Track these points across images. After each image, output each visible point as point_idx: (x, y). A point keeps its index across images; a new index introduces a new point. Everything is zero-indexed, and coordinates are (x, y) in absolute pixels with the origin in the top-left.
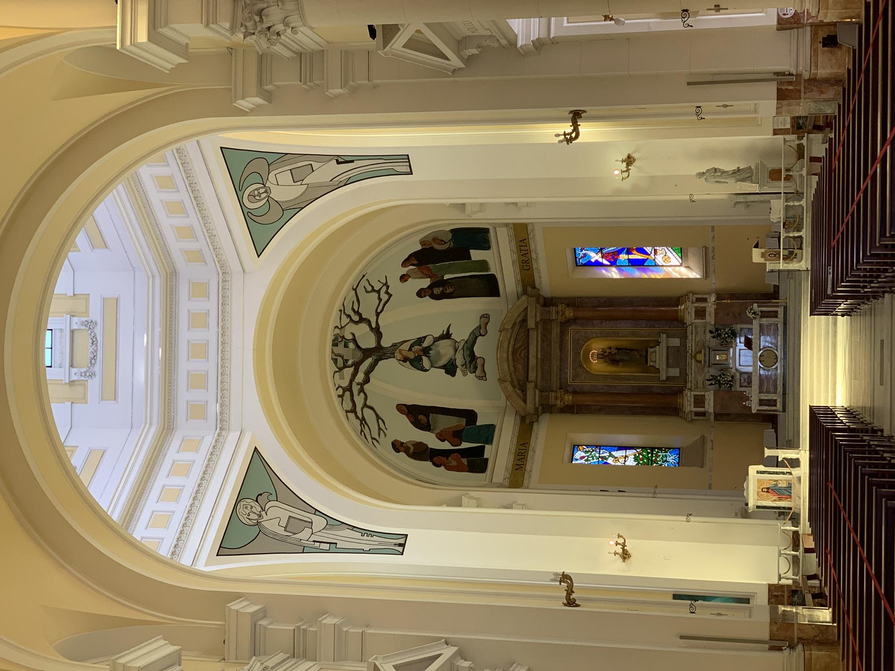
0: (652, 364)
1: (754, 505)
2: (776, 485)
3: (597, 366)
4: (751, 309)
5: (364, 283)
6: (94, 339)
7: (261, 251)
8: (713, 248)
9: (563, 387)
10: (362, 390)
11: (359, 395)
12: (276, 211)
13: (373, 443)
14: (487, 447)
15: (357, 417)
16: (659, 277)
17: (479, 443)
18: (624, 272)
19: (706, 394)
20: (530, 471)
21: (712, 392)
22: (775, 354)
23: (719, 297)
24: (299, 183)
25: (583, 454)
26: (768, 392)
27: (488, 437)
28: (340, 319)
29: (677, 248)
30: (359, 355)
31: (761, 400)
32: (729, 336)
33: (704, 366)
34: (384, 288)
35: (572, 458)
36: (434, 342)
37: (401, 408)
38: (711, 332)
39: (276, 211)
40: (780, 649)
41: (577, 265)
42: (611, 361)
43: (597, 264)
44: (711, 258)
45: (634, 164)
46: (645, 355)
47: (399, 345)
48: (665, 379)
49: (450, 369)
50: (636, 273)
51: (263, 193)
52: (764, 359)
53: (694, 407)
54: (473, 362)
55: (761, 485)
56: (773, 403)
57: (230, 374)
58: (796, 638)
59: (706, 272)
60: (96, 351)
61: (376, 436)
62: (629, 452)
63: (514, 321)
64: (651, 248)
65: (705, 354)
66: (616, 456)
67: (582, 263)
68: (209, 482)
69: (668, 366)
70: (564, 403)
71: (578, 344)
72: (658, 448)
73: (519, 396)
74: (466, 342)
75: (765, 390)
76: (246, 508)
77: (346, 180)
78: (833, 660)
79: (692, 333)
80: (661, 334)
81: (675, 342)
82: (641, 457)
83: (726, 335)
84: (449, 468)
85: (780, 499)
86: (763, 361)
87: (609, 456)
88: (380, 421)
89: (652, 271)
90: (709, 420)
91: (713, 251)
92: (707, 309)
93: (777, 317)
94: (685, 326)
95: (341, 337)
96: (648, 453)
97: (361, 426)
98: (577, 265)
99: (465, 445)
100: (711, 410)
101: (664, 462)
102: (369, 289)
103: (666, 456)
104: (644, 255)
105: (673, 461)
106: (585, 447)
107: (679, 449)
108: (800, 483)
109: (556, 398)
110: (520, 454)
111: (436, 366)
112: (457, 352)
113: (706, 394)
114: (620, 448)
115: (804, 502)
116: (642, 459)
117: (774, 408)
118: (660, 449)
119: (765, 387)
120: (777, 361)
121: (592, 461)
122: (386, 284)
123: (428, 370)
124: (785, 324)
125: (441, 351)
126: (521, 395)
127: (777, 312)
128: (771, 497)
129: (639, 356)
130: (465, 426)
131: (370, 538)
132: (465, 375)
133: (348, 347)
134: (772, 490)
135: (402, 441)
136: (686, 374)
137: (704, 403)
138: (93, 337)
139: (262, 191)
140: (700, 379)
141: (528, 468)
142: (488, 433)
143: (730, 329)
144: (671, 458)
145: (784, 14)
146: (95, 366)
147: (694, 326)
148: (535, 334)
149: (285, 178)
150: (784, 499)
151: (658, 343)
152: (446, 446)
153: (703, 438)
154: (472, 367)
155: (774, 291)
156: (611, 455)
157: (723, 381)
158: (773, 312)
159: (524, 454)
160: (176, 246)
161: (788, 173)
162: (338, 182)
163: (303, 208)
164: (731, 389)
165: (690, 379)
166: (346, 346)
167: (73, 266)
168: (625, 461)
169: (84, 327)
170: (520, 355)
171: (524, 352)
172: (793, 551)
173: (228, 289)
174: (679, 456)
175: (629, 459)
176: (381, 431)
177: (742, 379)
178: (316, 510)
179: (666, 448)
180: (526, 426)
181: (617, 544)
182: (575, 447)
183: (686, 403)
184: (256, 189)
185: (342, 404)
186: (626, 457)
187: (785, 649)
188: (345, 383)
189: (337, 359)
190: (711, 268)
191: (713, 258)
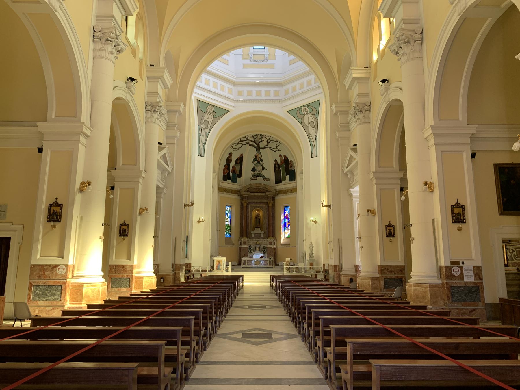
0: (255, 229)
5: (279, 144)
8: (290, 247)
10: (247, 143)
12: (300, 117)
14: (230, 181)
15: (239, 142)
23: (275, 249)
25: (229, 209)
31: (245, 261)
34: (277, 150)
38: (265, 246)
39: (300, 117)
40: (173, 267)
43: (285, 213)
49: (254, 170)
50: (282, 224)
54: (256, 176)
56: (244, 264)
60: (258, 62)
69: (255, 234)
71: (261, 207)
81: (262, 236)
85: (216, 267)
89: (283, 229)
90: (239, 246)
91: (289, 247)
93: (244, 265)
96: (229, 228)
99: (231, 174)
100: (242, 246)
102: (277, 145)
113: (247, 245)
114: (230, 220)
117: (243, 265)
118: (230, 232)
122: (279, 150)
124: (268, 268)
132: (252, 174)
136: (252, 239)
137: (244, 244)
139: (307, 112)
140: (251, 243)
142: (235, 181)
144: (228, 235)
145: (458, 270)
149: (311, 120)
151: (262, 231)
152: (231, 169)
154: (254, 176)
156: (228, 217)
160: (290, 86)
166: (260, 138)
169: (265, 58)
180: (237, 192)
181: (202, 219)
182: (231, 207)
183: (244, 239)
186: (228, 222)
188: (249, 138)
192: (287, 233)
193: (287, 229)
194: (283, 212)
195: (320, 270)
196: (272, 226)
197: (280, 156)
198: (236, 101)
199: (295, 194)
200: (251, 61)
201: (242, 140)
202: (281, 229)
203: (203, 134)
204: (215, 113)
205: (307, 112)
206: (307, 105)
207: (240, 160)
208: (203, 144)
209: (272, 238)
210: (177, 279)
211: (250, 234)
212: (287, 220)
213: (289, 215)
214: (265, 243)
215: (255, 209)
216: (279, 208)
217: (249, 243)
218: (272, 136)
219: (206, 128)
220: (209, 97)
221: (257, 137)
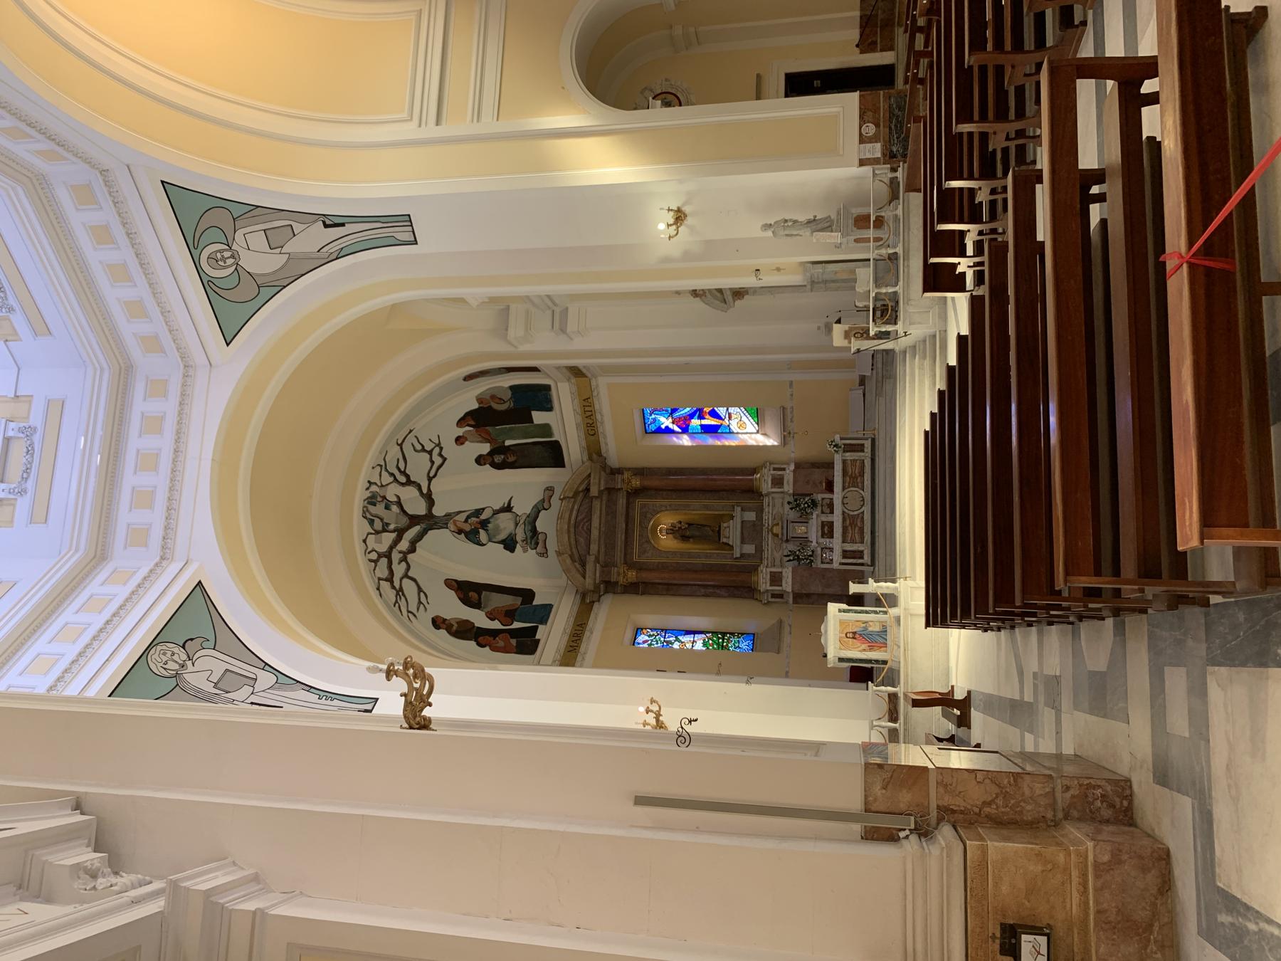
0: (725, 540)
1: (834, 656)
2: (865, 629)
3: (666, 542)
5: (411, 439)
6: (30, 449)
7: (232, 337)
8: (792, 408)
9: (631, 565)
10: (404, 559)
11: (399, 563)
12: (248, 289)
13: (408, 617)
14: (541, 627)
15: (393, 587)
17: (530, 623)
18: (696, 440)
20: (585, 653)
21: (790, 569)
24: (278, 250)
25: (647, 638)
26: (853, 541)
27: (544, 616)
28: (380, 476)
30: (404, 521)
31: (844, 551)
32: (809, 506)
34: (437, 450)
35: (634, 642)
36: (494, 514)
37: (449, 583)
38: (789, 503)
39: (248, 289)
40: (891, 837)
41: (646, 433)
43: (668, 431)
44: (789, 420)
45: (685, 222)
47: (453, 515)
48: (738, 555)
49: (509, 545)
50: (710, 441)
51: (228, 258)
53: (771, 585)
54: (534, 538)
55: (845, 628)
56: (860, 554)
57: (181, 490)
58: (933, 806)
60: (31, 463)
61: (413, 608)
66: (683, 640)
68: (123, 619)
69: (743, 542)
70: (627, 580)
71: (645, 517)
72: (730, 633)
73: (579, 571)
74: (528, 516)
76: (164, 654)
77: (337, 252)
78: (1049, 866)
79: (769, 505)
80: (735, 507)
81: (751, 516)
82: (711, 642)
83: (806, 505)
84: (494, 649)
85: (871, 648)
86: (847, 504)
87: (675, 641)
88: (422, 594)
89: (726, 439)
90: (787, 602)
91: (792, 412)
92: (785, 478)
93: (863, 451)
94: (762, 498)
95: (381, 497)
96: (719, 638)
97: (396, 597)
98: (646, 433)
99: (516, 625)
100: (789, 590)
102: (419, 447)
103: (739, 642)
107: (754, 634)
108: (899, 625)
109: (619, 574)
111: (494, 540)
113: (784, 571)
114: (688, 632)
115: (905, 650)
117: (860, 561)
118: (732, 634)
119: (850, 535)
120: (864, 504)
121: (656, 646)
122: (439, 445)
123: (485, 545)
124: (873, 460)
125: (501, 525)
126: (580, 569)
127: (863, 445)
128: (859, 645)
130: (521, 605)
131: (329, 702)
132: (525, 551)
133: (390, 510)
134: (860, 635)
135: (445, 618)
136: (762, 551)
137: (781, 581)
138: (30, 446)
139: (227, 254)
140: (778, 555)
141: (582, 649)
142: (544, 614)
144: (745, 645)
145: (867, 126)
146: (28, 482)
147: (771, 498)
148: (599, 504)
149: (258, 241)
150: (876, 648)
151: (732, 517)
152: (496, 625)
153: (781, 622)
154: (533, 543)
158: (858, 445)
160: (129, 329)
161: (878, 214)
162: (328, 254)
163: (285, 287)
164: (811, 565)
166: (387, 508)
167: (18, 362)
168: (693, 646)
169: (22, 435)
170: (583, 527)
171: (586, 524)
172: (889, 721)
173: (190, 385)
176: (422, 605)
178: (266, 664)
179: (739, 634)
180: (587, 603)
181: (648, 711)
182: (639, 630)
183: (761, 581)
184: (220, 251)
185: (374, 570)
186: (694, 641)
187: (907, 837)
188: (383, 548)
189: (374, 520)
191: (792, 421)
192: (741, 426)
193: (726, 420)
194: (665, 437)
195: (888, 182)
196: (715, 477)
197: (462, 440)
198: (165, 556)
199: (597, 386)
200: (22, 492)
201: (385, 574)
202: (727, 443)
203: (279, 698)
204: (192, 639)
205: (227, 254)
206: (193, 246)
207: (468, 592)
208: (323, 701)
210: (1006, 796)
211: (744, 562)
212: (695, 422)
214: (777, 507)
215: (652, 542)
216: (649, 452)
217: (777, 562)
218: (372, 456)
219: (252, 682)
220: (106, 658)
221: (382, 520)
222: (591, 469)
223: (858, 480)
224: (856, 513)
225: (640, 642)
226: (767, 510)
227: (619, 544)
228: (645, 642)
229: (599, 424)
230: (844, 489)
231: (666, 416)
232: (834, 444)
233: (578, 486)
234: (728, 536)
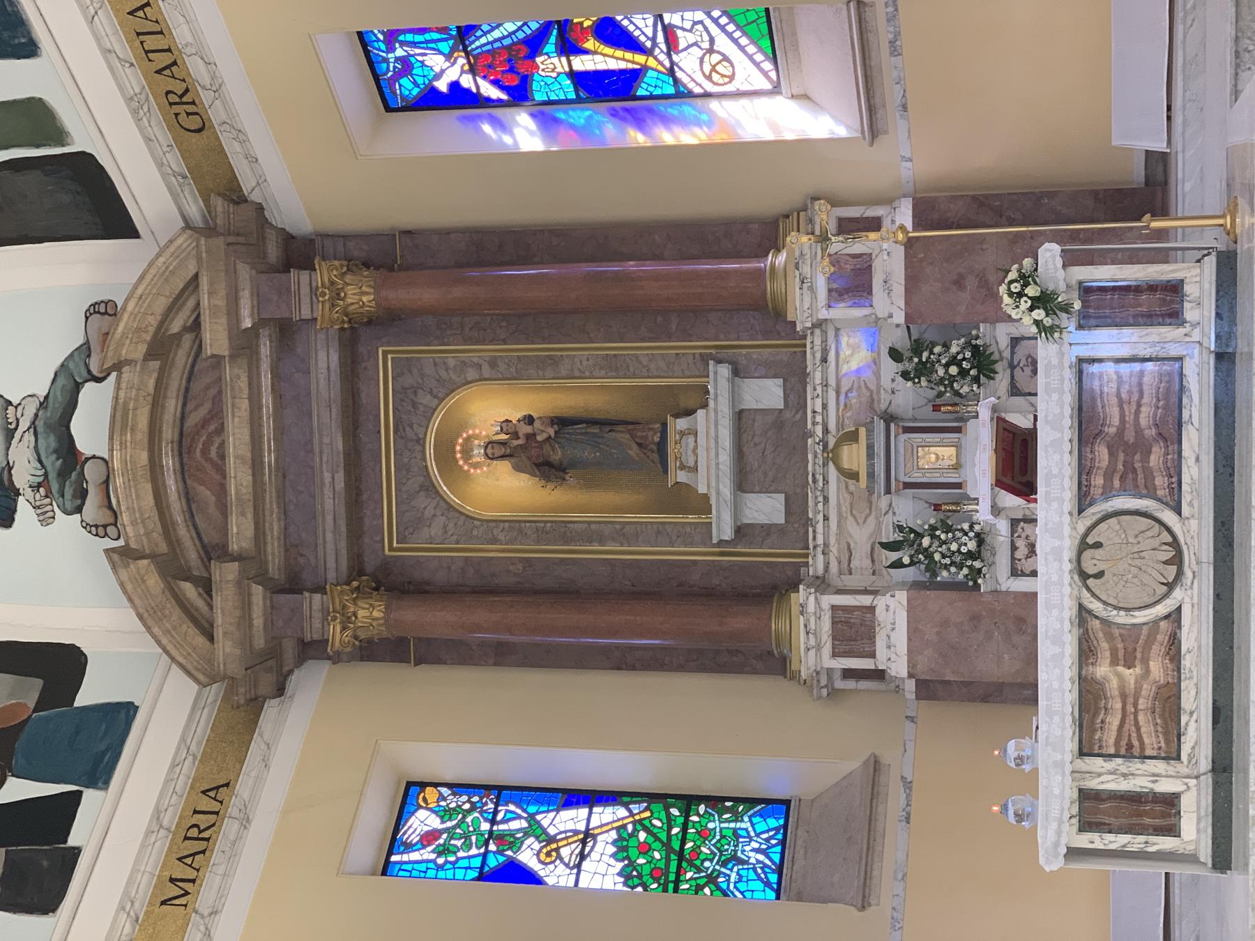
0: (682, 477)
4: (1025, 279)
14: (90, 797)
16: (695, 141)
19: (881, 602)
20: (214, 913)
22: (1167, 538)
23: (927, 213)
25: (434, 822)
26: (1130, 751)
27: (104, 754)
29: (752, 16)
31: (1086, 796)
32: (963, 373)
33: (870, 490)
38: (895, 354)
42: (538, 465)
43: (459, 98)
44: (885, 49)
46: (659, 444)
52: (1101, 566)
53: (835, 655)
59: (871, 110)
62: (605, 815)
63: (152, 330)
64: (650, 21)
65: (870, 447)
67: (403, 98)
69: (743, 483)
74: (43, 404)
75: (1110, 737)
80: (711, 362)
82: (642, 836)
83: (953, 370)
86: (1100, 575)
87: (527, 835)
89: (667, 121)
93: (1174, 316)
100: (899, 667)
101: (724, 864)
104: (629, 55)
105: (761, 857)
106: (445, 791)
110: (194, 833)
112: (15, 442)
116: (644, 849)
117: (1165, 843)
119: (1114, 721)
120: (1180, 574)
127: (1174, 289)
129: (635, 447)
130: (34, 711)
132: (46, 519)
136: (807, 522)
137: (872, 638)
140: (861, 536)
143: (968, 344)
153: (875, 766)
154: (69, 492)
155: (1147, 183)
156: (534, 829)
157: (944, 556)
158: (1152, 288)
159: (205, 835)
165: (820, 540)
170: (205, 452)
174: (785, 835)
175: (600, 847)
177: (1021, 543)
179: (737, 800)
190: (891, 94)
191: (895, 50)
209: (781, 258)
213: (479, 42)
222: (199, 259)
223: (1153, 459)
224: (1141, 617)
225: (415, 838)
226: (818, 375)
227: (329, 504)
228: (429, 837)
229: (206, 97)
230: (1084, 500)
231: (445, 47)
232: (1031, 291)
233: (162, 323)
234: (691, 464)
